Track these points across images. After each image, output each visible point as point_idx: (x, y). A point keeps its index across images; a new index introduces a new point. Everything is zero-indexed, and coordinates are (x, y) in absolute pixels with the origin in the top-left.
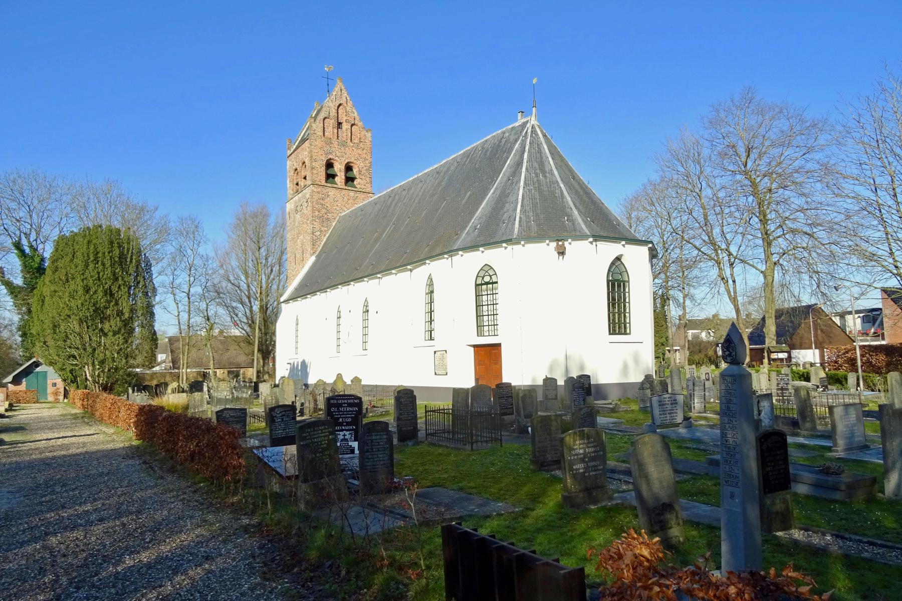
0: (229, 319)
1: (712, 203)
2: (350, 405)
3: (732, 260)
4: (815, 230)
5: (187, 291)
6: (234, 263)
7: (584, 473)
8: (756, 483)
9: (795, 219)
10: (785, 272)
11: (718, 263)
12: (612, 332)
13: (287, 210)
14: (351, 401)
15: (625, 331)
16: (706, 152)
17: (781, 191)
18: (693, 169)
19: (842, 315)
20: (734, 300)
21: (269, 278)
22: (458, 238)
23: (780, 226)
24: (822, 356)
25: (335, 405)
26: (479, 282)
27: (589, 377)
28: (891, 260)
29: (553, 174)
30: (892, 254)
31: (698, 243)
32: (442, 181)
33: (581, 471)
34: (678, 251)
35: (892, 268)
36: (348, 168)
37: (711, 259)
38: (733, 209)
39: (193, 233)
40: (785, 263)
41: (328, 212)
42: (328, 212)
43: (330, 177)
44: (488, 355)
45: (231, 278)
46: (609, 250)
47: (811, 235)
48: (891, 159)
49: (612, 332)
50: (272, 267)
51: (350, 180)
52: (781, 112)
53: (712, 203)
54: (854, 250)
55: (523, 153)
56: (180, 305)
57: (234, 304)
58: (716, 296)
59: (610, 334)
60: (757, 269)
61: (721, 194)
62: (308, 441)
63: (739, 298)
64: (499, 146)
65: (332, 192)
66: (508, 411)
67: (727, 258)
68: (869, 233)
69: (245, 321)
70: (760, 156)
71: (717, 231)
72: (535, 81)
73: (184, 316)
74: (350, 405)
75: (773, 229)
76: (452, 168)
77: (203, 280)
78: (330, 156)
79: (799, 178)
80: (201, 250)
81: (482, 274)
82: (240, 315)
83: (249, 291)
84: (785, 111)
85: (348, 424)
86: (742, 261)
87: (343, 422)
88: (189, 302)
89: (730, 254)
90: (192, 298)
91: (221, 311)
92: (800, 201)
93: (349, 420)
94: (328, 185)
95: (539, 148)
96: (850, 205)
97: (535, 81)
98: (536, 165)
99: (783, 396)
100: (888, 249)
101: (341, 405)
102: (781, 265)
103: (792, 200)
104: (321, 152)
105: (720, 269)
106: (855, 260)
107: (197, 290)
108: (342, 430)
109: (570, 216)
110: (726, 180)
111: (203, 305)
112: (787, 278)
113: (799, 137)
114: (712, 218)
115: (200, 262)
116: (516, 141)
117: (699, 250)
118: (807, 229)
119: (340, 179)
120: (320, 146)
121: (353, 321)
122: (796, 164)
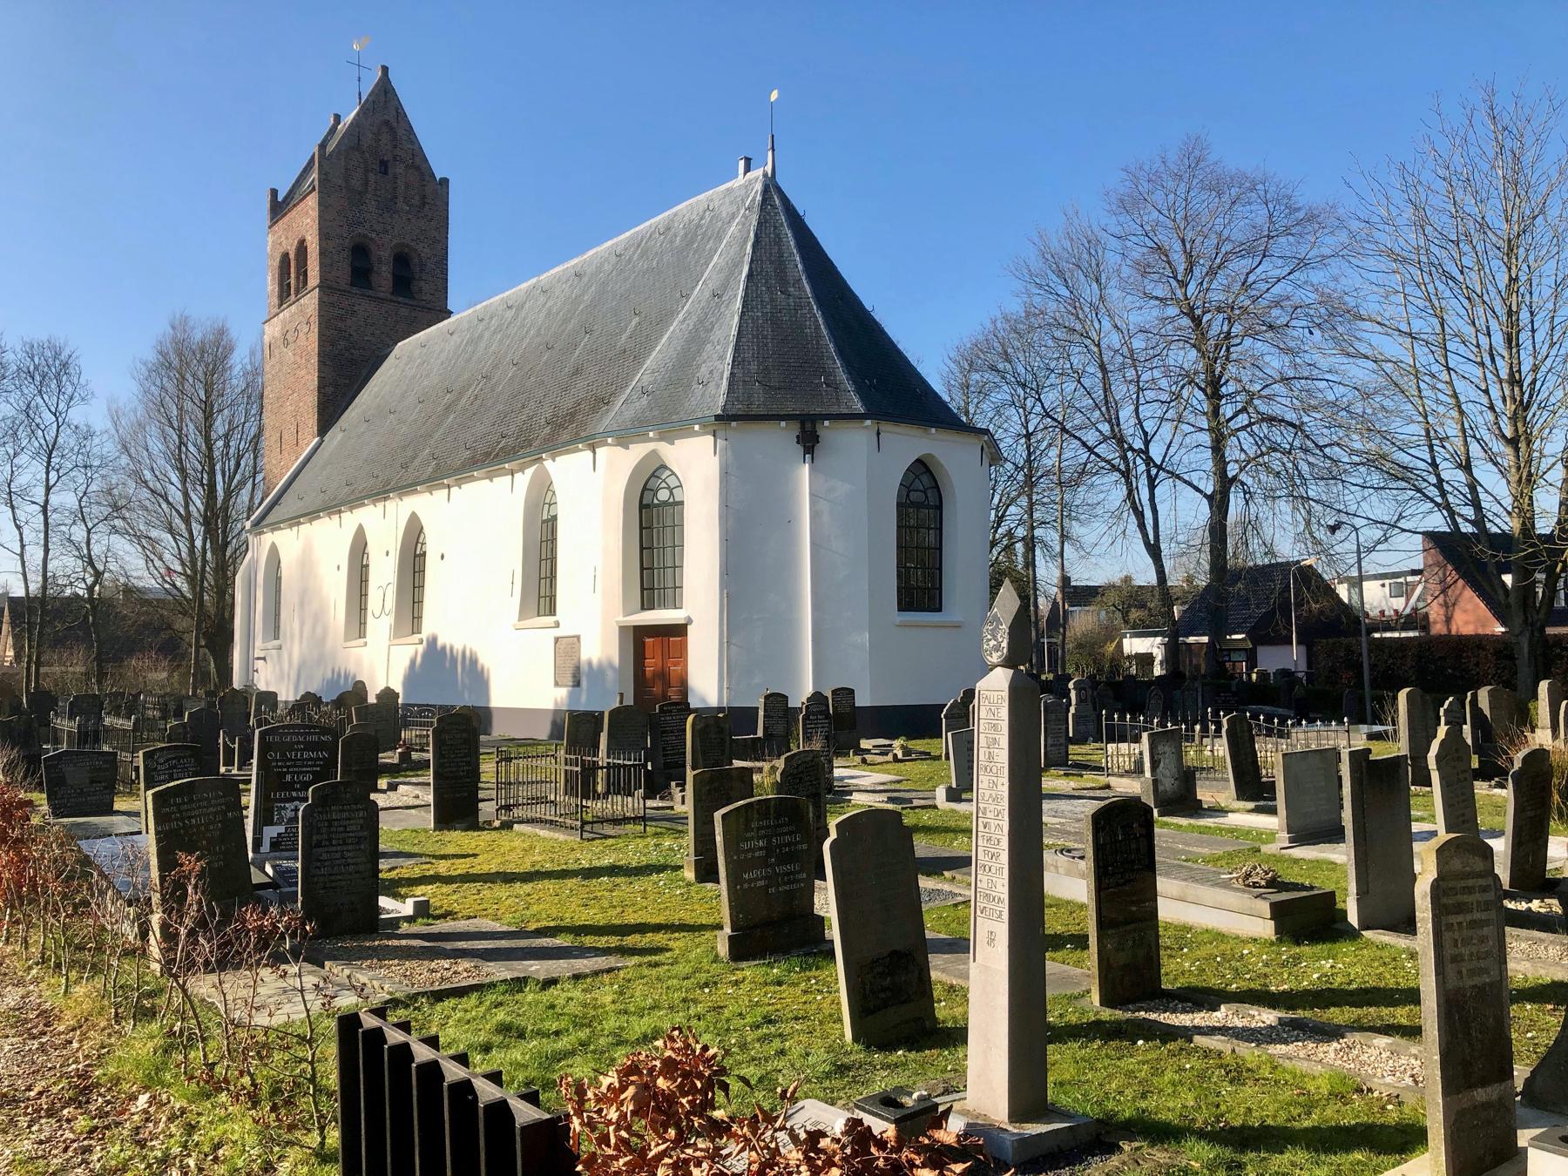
0: (142, 563)
1: (1119, 359)
3: (1154, 471)
4: (1306, 419)
5: (41, 501)
6: (156, 446)
7: (767, 887)
9: (1269, 398)
10: (1248, 496)
11: (1126, 474)
13: (267, 339)
16: (1112, 259)
17: (1248, 342)
18: (1089, 291)
19: (1357, 583)
20: (1154, 551)
21: (231, 479)
22: (608, 411)
23: (1244, 410)
27: (852, 692)
28: (1433, 479)
29: (801, 289)
30: (1434, 465)
31: (1091, 437)
32: (582, 295)
33: (761, 883)
34: (1054, 452)
35: (1433, 492)
36: (402, 260)
37: (1115, 468)
38: (1157, 374)
39: (58, 377)
40: (1249, 481)
45: (148, 475)
46: (908, 444)
47: (1298, 427)
48: (1441, 287)
50: (239, 459)
52: (1253, 189)
53: (1119, 359)
54: (1374, 461)
55: (745, 242)
56: (26, 531)
57: (154, 533)
58: (1119, 540)
60: (1197, 489)
61: (1138, 343)
62: (174, 825)
63: (1163, 546)
64: (698, 226)
67: (1142, 468)
68: (1396, 425)
69: (179, 569)
70: (1212, 272)
71: (1126, 413)
72: (774, 96)
73: (35, 554)
75: (1229, 414)
76: (607, 267)
77: (81, 479)
79: (1278, 316)
80: (76, 415)
82: (167, 556)
83: (187, 506)
84: (1260, 187)
86: (1174, 475)
87: (293, 782)
88: (46, 524)
89: (1149, 461)
90: (54, 518)
91: (121, 545)
92: (1275, 363)
94: (355, 290)
95: (778, 236)
96: (1361, 372)
97: (774, 96)
98: (769, 268)
100: (1427, 457)
101: (290, 747)
102: (1243, 484)
103: (1267, 358)
105: (1129, 484)
106: (1376, 479)
107: (64, 499)
108: (292, 800)
109: (829, 374)
110: (1149, 315)
111: (79, 533)
112: (1253, 508)
113: (1282, 240)
114: (1120, 390)
115: (72, 442)
116: (733, 217)
117: (1091, 450)
118: (1290, 416)
119: (384, 275)
122: (1276, 290)
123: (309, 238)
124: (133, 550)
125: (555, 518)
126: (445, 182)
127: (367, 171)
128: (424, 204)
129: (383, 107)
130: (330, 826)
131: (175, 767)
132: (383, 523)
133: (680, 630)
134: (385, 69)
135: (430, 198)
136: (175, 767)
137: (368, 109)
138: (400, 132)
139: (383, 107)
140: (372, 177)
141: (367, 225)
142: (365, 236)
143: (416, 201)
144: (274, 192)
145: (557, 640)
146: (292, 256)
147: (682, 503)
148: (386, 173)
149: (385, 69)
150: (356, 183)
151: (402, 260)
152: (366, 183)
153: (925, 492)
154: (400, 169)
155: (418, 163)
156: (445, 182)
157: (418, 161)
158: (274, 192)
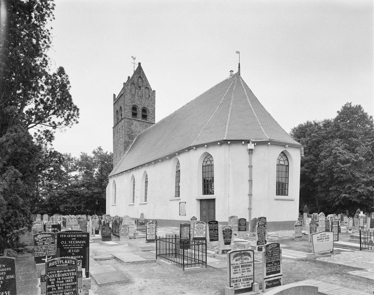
2: (78, 239)
8: (4, 25)
12: (278, 193)
14: (80, 236)
15: (285, 193)
24: (366, 212)
25: (64, 239)
26: (204, 165)
27: (265, 218)
36: (144, 110)
41: (132, 132)
42: (132, 132)
43: (135, 115)
44: (208, 205)
49: (278, 193)
51: (144, 117)
59: (276, 195)
65: (135, 123)
66: (215, 238)
74: (78, 239)
78: (134, 104)
81: (206, 160)
85: (76, 254)
93: (77, 251)
99: (173, 254)
101: (70, 239)
104: (129, 101)
120: (129, 98)
121: (140, 185)
123: (122, 106)
124: (312, 281)
125: (179, 171)
126: (154, 91)
127: (136, 89)
128: (149, 97)
129: (139, 71)
130: (56, 280)
131: (45, 240)
132: (139, 175)
133: (214, 200)
134: (140, 64)
135: (151, 95)
136: (45, 240)
137: (135, 72)
138: (143, 79)
139: (139, 71)
140: (137, 91)
141: (136, 102)
142: (135, 105)
143: (147, 96)
144: (114, 95)
145: (180, 203)
146: (119, 111)
147: (213, 165)
148: (140, 89)
149: (140, 64)
150: (133, 92)
151: (144, 110)
152: (136, 92)
153: (284, 161)
154: (143, 88)
155: (148, 87)
156: (154, 91)
157: (148, 86)
158: (114, 95)
